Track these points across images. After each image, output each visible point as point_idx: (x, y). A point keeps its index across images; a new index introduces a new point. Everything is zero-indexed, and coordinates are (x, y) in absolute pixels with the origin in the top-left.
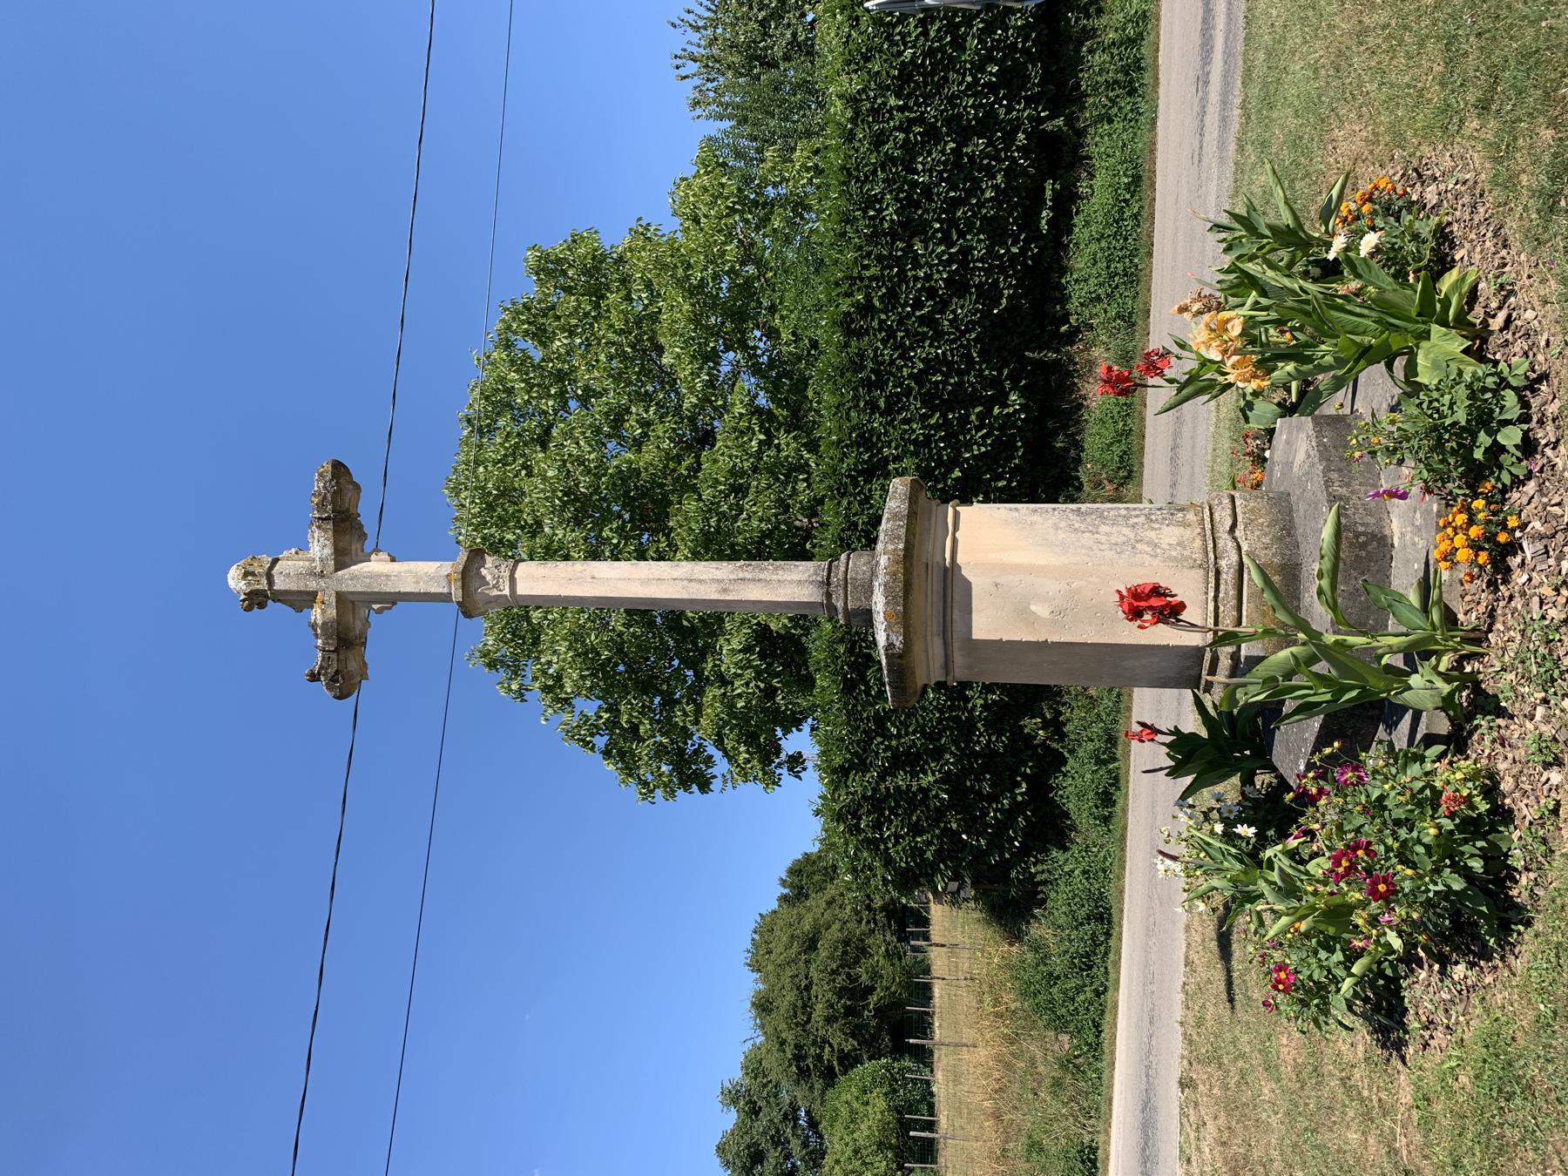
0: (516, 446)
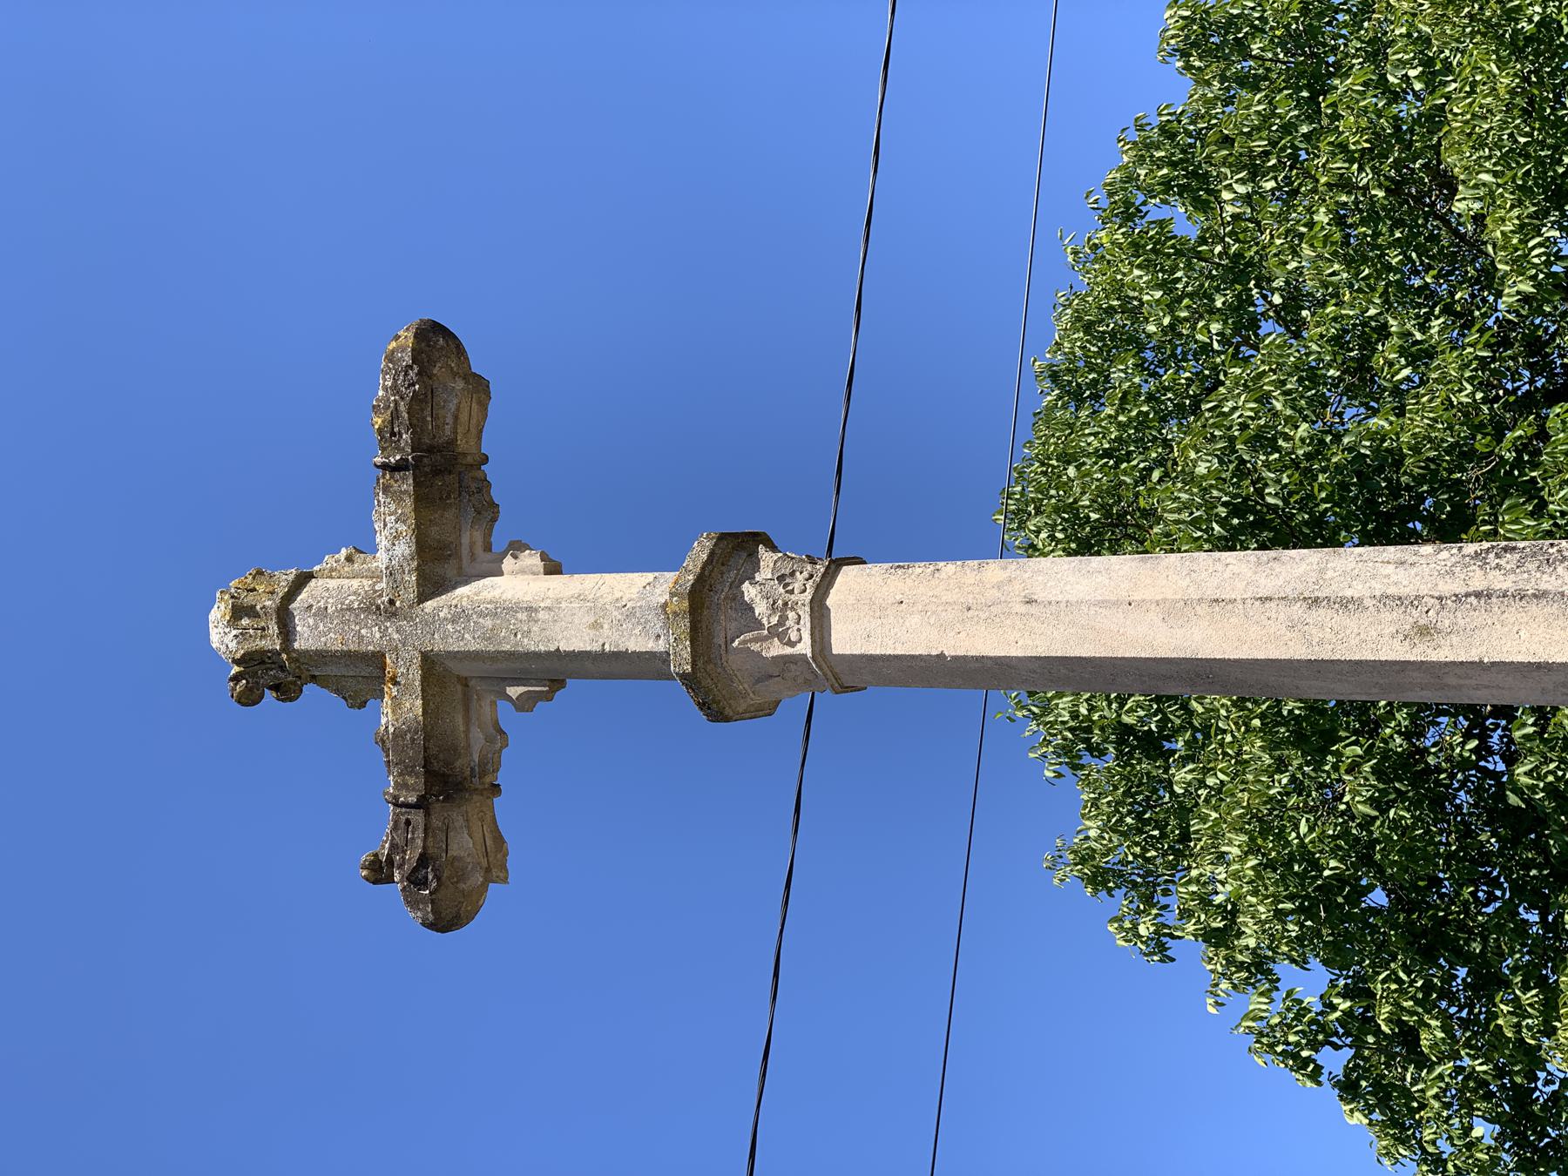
0: (1142, 422)
